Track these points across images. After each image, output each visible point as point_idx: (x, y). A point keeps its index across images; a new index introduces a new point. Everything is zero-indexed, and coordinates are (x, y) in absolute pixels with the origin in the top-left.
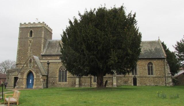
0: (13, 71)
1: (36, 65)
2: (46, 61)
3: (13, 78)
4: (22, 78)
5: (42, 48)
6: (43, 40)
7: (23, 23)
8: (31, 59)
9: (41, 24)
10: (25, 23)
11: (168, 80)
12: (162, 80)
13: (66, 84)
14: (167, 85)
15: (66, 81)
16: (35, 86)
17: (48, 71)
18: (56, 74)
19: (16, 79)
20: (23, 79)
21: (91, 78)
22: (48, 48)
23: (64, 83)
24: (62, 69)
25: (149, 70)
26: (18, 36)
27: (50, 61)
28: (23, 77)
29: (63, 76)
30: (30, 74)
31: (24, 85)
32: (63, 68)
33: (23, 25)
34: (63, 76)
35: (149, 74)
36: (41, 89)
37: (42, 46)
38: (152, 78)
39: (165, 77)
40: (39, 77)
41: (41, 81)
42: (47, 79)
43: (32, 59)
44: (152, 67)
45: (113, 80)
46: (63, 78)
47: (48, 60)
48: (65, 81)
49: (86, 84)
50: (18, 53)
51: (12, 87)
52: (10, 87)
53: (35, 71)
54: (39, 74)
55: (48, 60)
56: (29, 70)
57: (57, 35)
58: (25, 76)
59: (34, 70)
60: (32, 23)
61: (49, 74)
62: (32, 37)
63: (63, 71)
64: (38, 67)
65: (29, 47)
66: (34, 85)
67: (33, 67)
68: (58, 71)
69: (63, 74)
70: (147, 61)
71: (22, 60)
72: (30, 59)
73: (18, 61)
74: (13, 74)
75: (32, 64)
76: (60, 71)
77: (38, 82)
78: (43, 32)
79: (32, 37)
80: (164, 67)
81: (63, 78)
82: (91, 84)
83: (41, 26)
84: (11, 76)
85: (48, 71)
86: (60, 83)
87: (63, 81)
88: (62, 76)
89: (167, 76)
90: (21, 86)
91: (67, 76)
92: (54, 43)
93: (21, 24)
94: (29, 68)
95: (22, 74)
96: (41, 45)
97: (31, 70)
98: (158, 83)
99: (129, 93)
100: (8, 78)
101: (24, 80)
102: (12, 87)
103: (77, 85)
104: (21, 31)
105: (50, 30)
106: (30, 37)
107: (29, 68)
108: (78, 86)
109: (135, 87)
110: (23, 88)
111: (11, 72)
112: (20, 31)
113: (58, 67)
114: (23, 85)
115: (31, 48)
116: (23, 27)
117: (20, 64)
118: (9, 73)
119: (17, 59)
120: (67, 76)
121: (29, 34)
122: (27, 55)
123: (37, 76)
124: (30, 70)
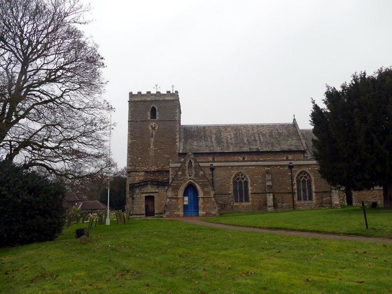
2: (209, 164)
5: (178, 140)
8: (190, 161)
15: (247, 200)
16: (203, 211)
24: (238, 179)
26: (128, 117)
29: (241, 191)
31: (181, 210)
33: (135, 95)
34: (241, 191)
36: (214, 215)
40: (209, 193)
45: (331, 197)
46: (241, 196)
49: (285, 205)
51: (143, 214)
56: (188, 182)
57: (306, 124)
59: (198, 183)
63: (240, 183)
65: (152, 139)
67: (196, 175)
68: (231, 183)
72: (189, 161)
73: (129, 166)
75: (193, 171)
76: (235, 182)
77: (207, 202)
81: (241, 196)
82: (294, 205)
83: (172, 98)
86: (236, 204)
90: (176, 213)
93: (131, 94)
94: (189, 178)
96: (176, 135)
99: (287, 225)
102: (143, 214)
104: (132, 109)
107: (189, 178)
108: (273, 208)
109: (350, 208)
110: (178, 216)
114: (179, 210)
115: (156, 141)
116: (136, 100)
119: (129, 162)
120: (250, 192)
121: (149, 113)
122: (149, 153)
123: (204, 193)
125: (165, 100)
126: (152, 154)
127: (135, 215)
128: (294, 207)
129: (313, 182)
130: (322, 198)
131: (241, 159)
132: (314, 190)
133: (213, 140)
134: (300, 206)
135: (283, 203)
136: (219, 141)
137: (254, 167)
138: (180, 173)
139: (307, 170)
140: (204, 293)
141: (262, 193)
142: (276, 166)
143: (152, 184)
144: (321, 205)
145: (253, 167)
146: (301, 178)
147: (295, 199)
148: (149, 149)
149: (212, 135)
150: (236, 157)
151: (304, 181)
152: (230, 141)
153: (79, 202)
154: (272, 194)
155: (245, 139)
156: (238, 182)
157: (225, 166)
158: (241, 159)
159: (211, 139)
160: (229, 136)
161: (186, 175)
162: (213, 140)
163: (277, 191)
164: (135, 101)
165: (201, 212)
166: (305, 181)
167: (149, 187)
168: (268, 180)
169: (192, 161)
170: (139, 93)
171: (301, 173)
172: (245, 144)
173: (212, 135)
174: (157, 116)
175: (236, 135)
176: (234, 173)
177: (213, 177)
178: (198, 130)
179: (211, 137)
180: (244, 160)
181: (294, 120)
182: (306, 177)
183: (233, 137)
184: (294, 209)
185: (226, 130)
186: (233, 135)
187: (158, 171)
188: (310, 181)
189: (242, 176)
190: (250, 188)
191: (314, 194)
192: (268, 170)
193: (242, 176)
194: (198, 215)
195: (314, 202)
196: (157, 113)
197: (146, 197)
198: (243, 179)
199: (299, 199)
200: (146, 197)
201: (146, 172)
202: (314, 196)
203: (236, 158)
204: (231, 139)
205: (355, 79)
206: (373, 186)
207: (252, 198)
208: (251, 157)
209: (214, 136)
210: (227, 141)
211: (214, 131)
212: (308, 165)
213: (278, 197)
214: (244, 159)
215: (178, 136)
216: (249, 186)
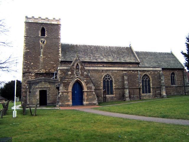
8: (77, 64)
13: (112, 97)
14: (187, 94)
15: (112, 93)
20: (68, 92)
25: (172, 79)
28: (67, 90)
29: (108, 87)
30: (78, 86)
35: (172, 84)
38: (175, 88)
39: (184, 87)
44: (174, 77)
45: (160, 90)
48: (146, 93)
49: (135, 96)
50: (24, 58)
53: (85, 81)
56: (76, 80)
62: (45, 36)
63: (108, 81)
65: (42, 50)
67: (82, 75)
69: (146, 84)
70: (171, 71)
71: (31, 66)
75: (80, 71)
76: (104, 81)
79: (45, 36)
80: (184, 77)
81: (108, 90)
82: (140, 96)
89: (186, 85)
100: (30, 92)
106: (41, 36)
107: (76, 77)
108: (129, 98)
114: (69, 101)
115: (44, 52)
117: (30, 73)
120: (114, 87)
122: (39, 60)
123: (88, 88)
125: (52, 24)
126: (41, 60)
128: (140, 98)
129: (151, 81)
130: (156, 91)
132: (151, 86)
138: (70, 73)
139: (147, 73)
142: (130, 70)
143: (45, 81)
144: (155, 96)
145: (116, 71)
146: (144, 78)
147: (141, 92)
151: (108, 81)
154: (128, 89)
156: (106, 81)
161: (74, 75)
165: (85, 103)
166: (109, 82)
169: (79, 64)
171: (106, 76)
174: (46, 34)
176: (104, 74)
180: (104, 67)
181: (130, 44)
182: (147, 78)
184: (140, 99)
187: (46, 73)
188: (149, 81)
189: (109, 76)
191: (151, 89)
192: (125, 73)
193: (109, 76)
196: (46, 32)
198: (109, 79)
202: (151, 90)
205: (60, 33)
206: (5, 86)
212: (148, 71)
216: (114, 84)
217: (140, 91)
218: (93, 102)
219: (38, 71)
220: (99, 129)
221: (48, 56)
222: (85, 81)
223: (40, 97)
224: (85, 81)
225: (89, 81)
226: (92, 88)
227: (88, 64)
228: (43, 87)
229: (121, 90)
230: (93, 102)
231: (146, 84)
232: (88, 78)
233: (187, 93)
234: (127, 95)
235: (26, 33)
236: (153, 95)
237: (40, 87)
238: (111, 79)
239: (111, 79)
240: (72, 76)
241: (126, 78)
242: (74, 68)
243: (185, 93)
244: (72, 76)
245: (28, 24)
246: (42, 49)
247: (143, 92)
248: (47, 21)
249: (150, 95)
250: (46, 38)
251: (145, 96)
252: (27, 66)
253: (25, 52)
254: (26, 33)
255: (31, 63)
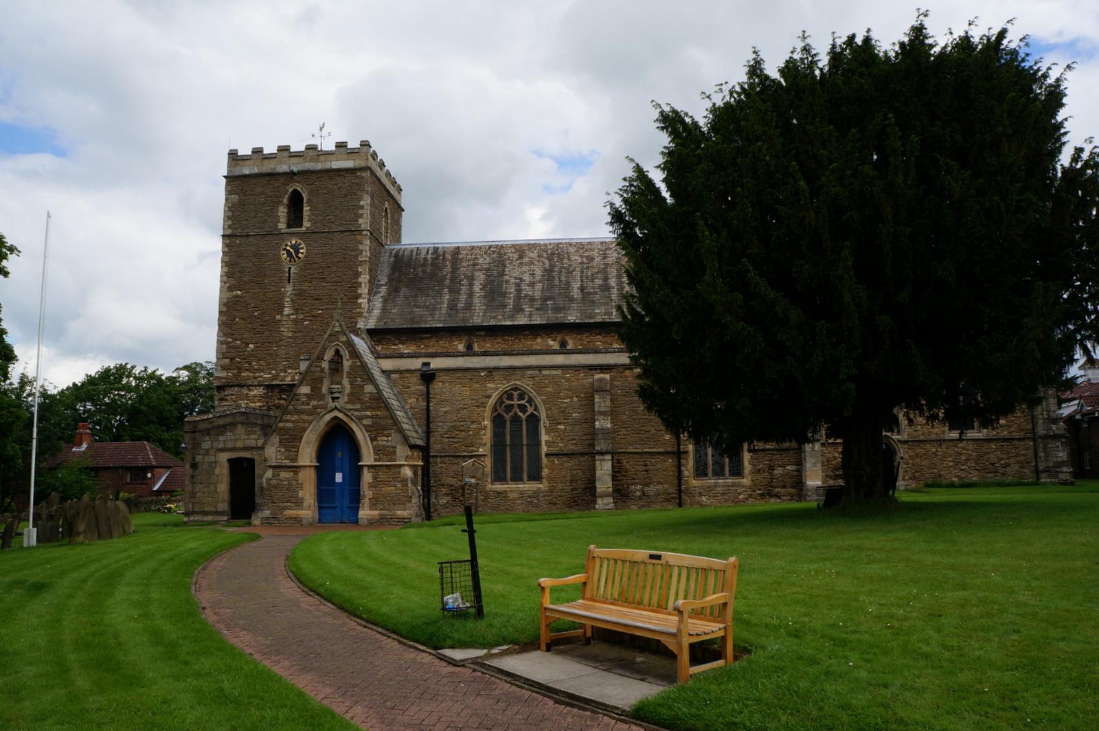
0: (221, 422)
1: (369, 388)
2: (417, 364)
3: (226, 465)
4: (287, 462)
5: (364, 290)
6: (366, 246)
7: (245, 151)
8: (337, 352)
9: (353, 152)
10: (257, 151)
11: (1047, 455)
12: (1017, 455)
13: (536, 494)
15: (535, 476)
16: (373, 506)
17: (428, 421)
18: (477, 434)
19: (243, 471)
20: (296, 469)
21: (679, 455)
22: (397, 290)
23: (527, 486)
24: (509, 408)
27: (436, 363)
28: (295, 459)
32: (516, 402)
33: (245, 159)
37: (364, 279)
39: (1034, 440)
40: (391, 453)
41: (404, 481)
42: (423, 467)
43: (345, 354)
47: (426, 360)
48: (512, 480)
49: (651, 490)
50: (222, 324)
52: (209, 518)
54: (393, 439)
55: (426, 360)
56: (328, 417)
57: (605, 232)
58: (307, 455)
60: (270, 149)
61: (432, 439)
63: (516, 420)
64: (378, 400)
65: (289, 289)
66: (366, 502)
67: (355, 397)
73: (224, 368)
74: (225, 439)
75: (346, 382)
76: (498, 421)
77: (386, 483)
78: (366, 201)
79: (301, 226)
82: (680, 491)
83: (349, 164)
84: (207, 452)
85: (428, 421)
86: (499, 487)
87: (723, 475)
88: (512, 446)
89: (1041, 430)
91: (539, 444)
92: (425, 259)
93: (233, 156)
94: (331, 405)
95: (291, 440)
96: (358, 274)
97: (341, 415)
98: (1001, 470)
101: (302, 475)
103: (602, 497)
104: (235, 198)
105: (393, 190)
110: (297, 521)
111: (208, 432)
112: (229, 193)
113: (489, 397)
115: (300, 294)
117: (241, 386)
118: (197, 435)
120: (544, 449)
121: (282, 211)
122: (278, 332)
123: (377, 451)
124: (336, 413)
126: (286, 332)
127: (197, 513)
130: (771, 468)
131: (555, 345)
133: (477, 287)
134: (701, 494)
135: (647, 485)
136: (494, 292)
137: (559, 372)
138: (305, 390)
140: (766, 730)
141: (582, 454)
143: (246, 424)
145: (554, 372)
147: (686, 473)
148: (278, 317)
149: (477, 274)
150: (539, 340)
152: (527, 290)
153: (157, 470)
154: (609, 457)
155: (576, 285)
157: (467, 369)
158: (555, 345)
159: (471, 285)
160: (529, 275)
161: (322, 397)
162: (477, 287)
163: (631, 449)
164: (246, 176)
165: (365, 513)
167: (240, 430)
168: (601, 413)
170: (257, 151)
172: (571, 299)
173: (477, 274)
175: (549, 272)
176: (497, 389)
177: (428, 402)
178: (437, 258)
179: (471, 279)
183: (538, 278)
185: (521, 257)
186: (539, 273)
189: (521, 397)
190: (544, 437)
193: (521, 397)
194: (356, 522)
195: (746, 481)
196: (306, 208)
197: (230, 461)
198: (523, 408)
199: (701, 472)
200: (230, 461)
201: (270, 387)
203: (539, 343)
204: (532, 284)
207: (551, 469)
208: (585, 339)
209: (480, 277)
210: (519, 291)
211: (484, 261)
213: (627, 464)
214: (563, 344)
215: (364, 279)
216: (543, 431)
217: (679, 465)
218: (399, 513)
219: (275, 377)
220: (572, 635)
221: (314, 313)
222: (365, 422)
223: (254, 482)
224: (365, 422)
225: (383, 422)
226: (394, 453)
227: (485, 336)
228: (239, 444)
229: (582, 459)
230: (399, 513)
231: (516, 435)
232: (378, 408)
233: (1050, 476)
234: (604, 483)
235: (230, 222)
236: (753, 488)
237: (230, 445)
238: (530, 410)
239: (530, 410)
240: (314, 403)
241: (601, 403)
242: (322, 370)
243: (1037, 472)
244: (314, 403)
245: (235, 182)
246: (289, 282)
247: (701, 472)
248: (312, 160)
249: (739, 485)
250: (305, 236)
251: (708, 490)
252: (232, 359)
253: (225, 300)
254: (230, 222)
255: (247, 344)
